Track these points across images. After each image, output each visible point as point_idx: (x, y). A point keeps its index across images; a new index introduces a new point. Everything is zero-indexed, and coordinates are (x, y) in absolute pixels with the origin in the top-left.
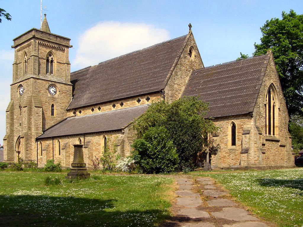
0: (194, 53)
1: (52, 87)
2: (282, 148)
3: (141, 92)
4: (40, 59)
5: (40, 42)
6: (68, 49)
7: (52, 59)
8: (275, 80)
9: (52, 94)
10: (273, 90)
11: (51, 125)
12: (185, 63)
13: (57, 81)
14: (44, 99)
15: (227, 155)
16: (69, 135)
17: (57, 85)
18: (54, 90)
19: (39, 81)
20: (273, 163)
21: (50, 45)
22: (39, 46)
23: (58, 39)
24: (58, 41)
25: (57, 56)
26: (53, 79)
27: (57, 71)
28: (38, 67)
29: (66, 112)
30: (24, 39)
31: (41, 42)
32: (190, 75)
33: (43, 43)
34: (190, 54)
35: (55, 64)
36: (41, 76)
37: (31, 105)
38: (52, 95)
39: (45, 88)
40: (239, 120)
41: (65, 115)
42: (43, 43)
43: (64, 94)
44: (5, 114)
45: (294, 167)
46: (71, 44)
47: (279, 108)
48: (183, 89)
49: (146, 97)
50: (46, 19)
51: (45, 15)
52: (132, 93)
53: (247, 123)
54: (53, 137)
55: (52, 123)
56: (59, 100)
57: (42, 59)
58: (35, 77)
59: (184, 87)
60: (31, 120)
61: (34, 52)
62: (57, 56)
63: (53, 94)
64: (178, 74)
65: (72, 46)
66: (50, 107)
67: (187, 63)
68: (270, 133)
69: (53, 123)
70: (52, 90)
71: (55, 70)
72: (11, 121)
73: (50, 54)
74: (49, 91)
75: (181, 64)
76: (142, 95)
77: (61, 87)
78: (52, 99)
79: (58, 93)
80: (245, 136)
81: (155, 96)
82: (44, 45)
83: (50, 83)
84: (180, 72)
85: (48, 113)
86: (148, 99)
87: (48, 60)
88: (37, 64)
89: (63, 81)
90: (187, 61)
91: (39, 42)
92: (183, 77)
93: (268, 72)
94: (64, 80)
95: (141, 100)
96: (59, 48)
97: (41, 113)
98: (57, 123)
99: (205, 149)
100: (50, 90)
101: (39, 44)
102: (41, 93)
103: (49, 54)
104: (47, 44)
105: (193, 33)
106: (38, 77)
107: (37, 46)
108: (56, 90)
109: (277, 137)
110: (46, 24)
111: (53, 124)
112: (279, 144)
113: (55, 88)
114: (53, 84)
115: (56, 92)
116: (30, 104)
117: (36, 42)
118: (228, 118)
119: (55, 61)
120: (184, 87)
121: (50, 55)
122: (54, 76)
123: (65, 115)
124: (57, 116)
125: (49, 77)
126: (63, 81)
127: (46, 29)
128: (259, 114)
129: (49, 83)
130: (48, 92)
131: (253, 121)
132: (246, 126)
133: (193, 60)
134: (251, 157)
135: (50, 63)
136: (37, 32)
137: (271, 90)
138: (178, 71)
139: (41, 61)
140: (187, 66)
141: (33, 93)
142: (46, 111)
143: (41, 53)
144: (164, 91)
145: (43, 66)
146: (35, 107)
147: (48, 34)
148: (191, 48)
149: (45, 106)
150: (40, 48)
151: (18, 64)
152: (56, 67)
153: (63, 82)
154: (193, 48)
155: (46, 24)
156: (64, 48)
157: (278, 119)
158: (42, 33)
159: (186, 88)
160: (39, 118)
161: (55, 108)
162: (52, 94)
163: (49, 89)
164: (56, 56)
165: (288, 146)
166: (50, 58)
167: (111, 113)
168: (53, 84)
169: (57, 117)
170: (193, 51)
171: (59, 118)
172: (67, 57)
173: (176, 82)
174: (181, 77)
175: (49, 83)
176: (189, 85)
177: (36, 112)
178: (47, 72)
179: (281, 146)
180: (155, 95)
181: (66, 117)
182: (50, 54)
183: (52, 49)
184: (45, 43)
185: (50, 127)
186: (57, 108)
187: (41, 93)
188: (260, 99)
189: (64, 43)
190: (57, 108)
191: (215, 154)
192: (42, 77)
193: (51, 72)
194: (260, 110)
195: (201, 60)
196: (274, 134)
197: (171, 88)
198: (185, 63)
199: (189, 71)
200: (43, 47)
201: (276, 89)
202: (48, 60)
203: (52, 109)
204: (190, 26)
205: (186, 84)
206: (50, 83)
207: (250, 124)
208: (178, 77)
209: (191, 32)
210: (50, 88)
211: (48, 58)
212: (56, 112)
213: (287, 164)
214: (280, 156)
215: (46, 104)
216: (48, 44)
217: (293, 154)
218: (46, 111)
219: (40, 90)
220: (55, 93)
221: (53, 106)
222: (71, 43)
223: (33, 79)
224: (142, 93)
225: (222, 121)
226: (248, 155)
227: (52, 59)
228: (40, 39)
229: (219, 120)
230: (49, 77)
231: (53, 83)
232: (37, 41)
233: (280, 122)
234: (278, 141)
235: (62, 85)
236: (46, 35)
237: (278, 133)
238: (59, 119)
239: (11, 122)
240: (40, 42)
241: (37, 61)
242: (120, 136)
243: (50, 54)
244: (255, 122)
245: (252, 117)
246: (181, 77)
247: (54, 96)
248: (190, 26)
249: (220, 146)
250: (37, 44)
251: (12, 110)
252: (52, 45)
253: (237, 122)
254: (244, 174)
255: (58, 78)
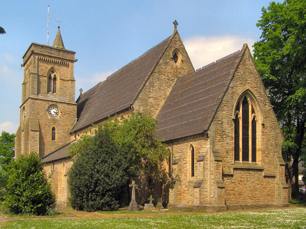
0: (180, 58)
1: (53, 108)
2: (270, 180)
4: (40, 77)
5: (39, 58)
6: (73, 64)
7: (55, 76)
8: (254, 85)
9: (53, 116)
10: (252, 99)
11: (51, 151)
12: (166, 70)
13: (58, 101)
14: (42, 122)
15: (186, 190)
17: (60, 105)
18: (55, 111)
19: (38, 101)
20: (251, 201)
21: (52, 60)
22: (40, 62)
23: (61, 53)
24: (61, 55)
25: (61, 72)
26: (54, 99)
27: (60, 89)
28: (37, 86)
29: (69, 136)
30: (28, 55)
31: (42, 58)
32: (173, 85)
33: (44, 58)
34: (175, 58)
35: (58, 82)
36: (40, 96)
37: (28, 129)
38: (54, 117)
39: (45, 109)
40: (196, 143)
41: (68, 139)
42: (44, 58)
43: (67, 115)
45: (286, 206)
46: (76, 58)
47: (263, 125)
48: (162, 103)
50: (59, 32)
51: (59, 27)
53: (204, 146)
55: (53, 149)
56: (61, 123)
57: (43, 77)
58: (33, 97)
59: (164, 101)
60: (28, 146)
61: (33, 69)
62: (61, 72)
63: (55, 116)
64: (155, 84)
65: (76, 61)
66: (50, 131)
67: (169, 71)
68: (246, 158)
69: (54, 148)
70: (53, 111)
71: (58, 88)
72: (18, 147)
73: (52, 70)
74: (50, 112)
75: (159, 72)
77: (64, 108)
78: (53, 121)
79: (60, 114)
80: (200, 164)
82: (44, 61)
83: (51, 103)
84: (158, 82)
85: (48, 138)
87: (50, 78)
88: (36, 83)
89: (67, 100)
90: (168, 68)
91: (38, 58)
92: (162, 88)
93: (239, 74)
94: (68, 99)
96: (63, 63)
97: (38, 137)
98: (59, 148)
99: (169, 181)
100: (50, 111)
101: (39, 60)
102: (40, 115)
103: (52, 70)
104: (48, 59)
105: (178, 31)
106: (36, 98)
107: (37, 62)
108: (57, 111)
109: (259, 163)
110: (60, 38)
111: (54, 150)
112: (263, 174)
113: (56, 109)
114: (54, 104)
115: (57, 113)
116: (27, 128)
117: (35, 58)
118: (187, 139)
119: (58, 78)
120: (164, 101)
121: (53, 72)
122: (56, 95)
123: (68, 139)
124: (59, 140)
125: (51, 97)
126: (67, 100)
127: (58, 43)
128: (222, 134)
129: (49, 104)
130: (47, 113)
131: (209, 144)
132: (203, 150)
133: (179, 67)
134: (205, 193)
135: (52, 81)
136: (36, 47)
137: (249, 99)
138: (154, 81)
139: (41, 79)
140: (169, 74)
141: (30, 116)
142: (46, 135)
143: (42, 70)
144: (133, 107)
145: (44, 85)
146: (32, 130)
147: (49, 48)
148: (176, 51)
149: (45, 129)
150: (40, 64)
151: (26, 84)
152: (59, 84)
153: (66, 102)
154: (179, 51)
155: (60, 38)
156: (68, 63)
157: (260, 140)
158: (42, 48)
159: (166, 102)
160: (36, 143)
161: (56, 132)
162: (53, 116)
163: (50, 110)
164: (59, 73)
165: (278, 176)
166: (53, 76)
168: (54, 104)
169: (58, 141)
170: (180, 54)
171: (61, 143)
172: (72, 74)
173: (151, 96)
174: (159, 89)
175: (49, 104)
176: (170, 99)
177: (32, 137)
178: (49, 91)
179: (265, 177)
181: (69, 142)
182: (53, 71)
183: (55, 65)
184: (46, 59)
185: (50, 153)
186: (58, 132)
187: (40, 115)
188: (224, 112)
189: (68, 57)
190: (58, 132)
191: (172, 188)
192: (42, 97)
193: (54, 91)
194: (223, 127)
195: (192, 65)
196: (254, 159)
197: (143, 103)
198: (166, 70)
199: (173, 80)
201: (257, 98)
202: (50, 78)
203: (52, 133)
204: (176, 23)
205: (167, 97)
206: (51, 103)
207: (205, 147)
208: (154, 89)
209: (176, 31)
210: (51, 109)
211: (50, 75)
212: (57, 136)
213: (277, 201)
214: (265, 191)
215: (46, 127)
216: (50, 59)
217: (284, 188)
218: (46, 135)
219: (39, 112)
220: (57, 114)
221: (54, 129)
222: (76, 57)
223: (31, 100)
225: (182, 143)
226: (200, 191)
227: (55, 76)
228: (40, 54)
229: (180, 143)
230: (51, 97)
231: (54, 103)
232: (37, 57)
233: (266, 143)
234: (261, 170)
235: (64, 105)
236: (47, 50)
237: (260, 159)
238: (61, 144)
239: (18, 148)
240: (39, 58)
241: (36, 80)
243: (52, 70)
244: (213, 144)
245: (208, 137)
246: (159, 89)
247: (56, 118)
248: (176, 23)
249: (180, 176)
250: (37, 60)
251: (19, 135)
252: (54, 60)
253: (195, 144)
255: (62, 98)
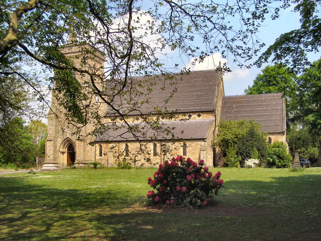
3: (193, 109)
16: (198, 139)
44: (278, 36)
49: (197, 114)
52: (197, 108)
54: (119, 141)
76: (194, 112)
81: (206, 114)
86: (199, 116)
95: (192, 115)
167: (194, 122)
180: (206, 113)
200: (38, 140)
204: (245, 61)
224: (194, 111)
242: (203, 143)
248: (245, 61)
254: (285, 184)
